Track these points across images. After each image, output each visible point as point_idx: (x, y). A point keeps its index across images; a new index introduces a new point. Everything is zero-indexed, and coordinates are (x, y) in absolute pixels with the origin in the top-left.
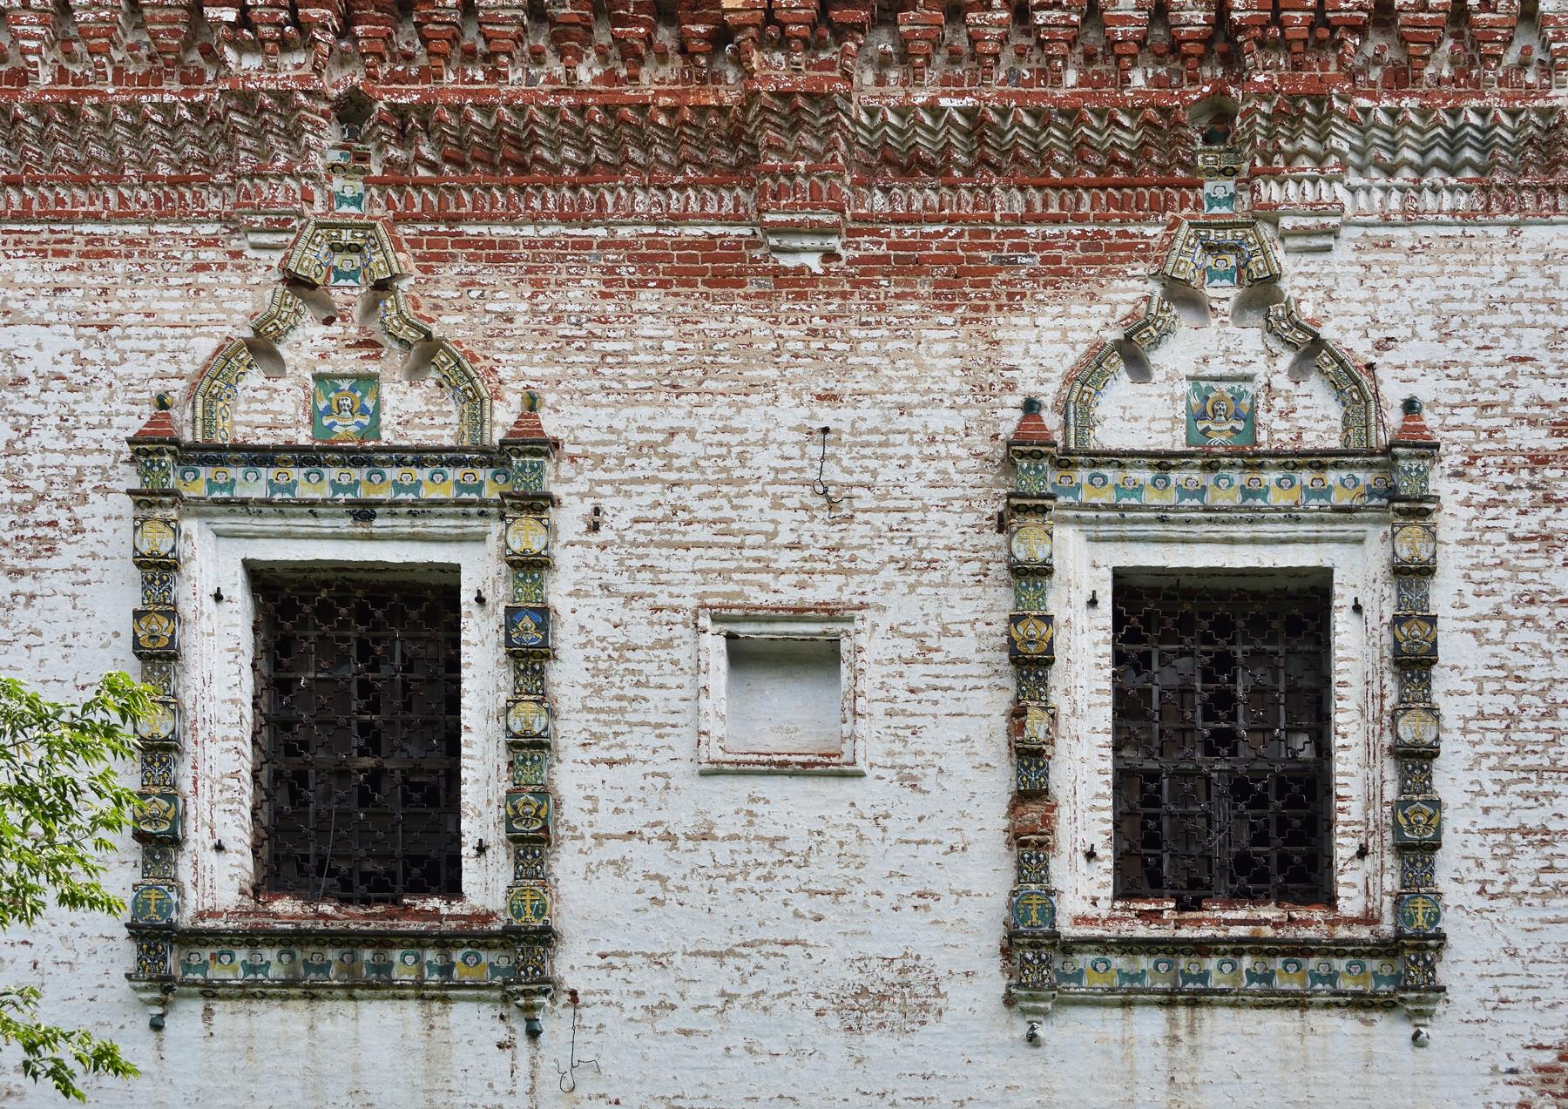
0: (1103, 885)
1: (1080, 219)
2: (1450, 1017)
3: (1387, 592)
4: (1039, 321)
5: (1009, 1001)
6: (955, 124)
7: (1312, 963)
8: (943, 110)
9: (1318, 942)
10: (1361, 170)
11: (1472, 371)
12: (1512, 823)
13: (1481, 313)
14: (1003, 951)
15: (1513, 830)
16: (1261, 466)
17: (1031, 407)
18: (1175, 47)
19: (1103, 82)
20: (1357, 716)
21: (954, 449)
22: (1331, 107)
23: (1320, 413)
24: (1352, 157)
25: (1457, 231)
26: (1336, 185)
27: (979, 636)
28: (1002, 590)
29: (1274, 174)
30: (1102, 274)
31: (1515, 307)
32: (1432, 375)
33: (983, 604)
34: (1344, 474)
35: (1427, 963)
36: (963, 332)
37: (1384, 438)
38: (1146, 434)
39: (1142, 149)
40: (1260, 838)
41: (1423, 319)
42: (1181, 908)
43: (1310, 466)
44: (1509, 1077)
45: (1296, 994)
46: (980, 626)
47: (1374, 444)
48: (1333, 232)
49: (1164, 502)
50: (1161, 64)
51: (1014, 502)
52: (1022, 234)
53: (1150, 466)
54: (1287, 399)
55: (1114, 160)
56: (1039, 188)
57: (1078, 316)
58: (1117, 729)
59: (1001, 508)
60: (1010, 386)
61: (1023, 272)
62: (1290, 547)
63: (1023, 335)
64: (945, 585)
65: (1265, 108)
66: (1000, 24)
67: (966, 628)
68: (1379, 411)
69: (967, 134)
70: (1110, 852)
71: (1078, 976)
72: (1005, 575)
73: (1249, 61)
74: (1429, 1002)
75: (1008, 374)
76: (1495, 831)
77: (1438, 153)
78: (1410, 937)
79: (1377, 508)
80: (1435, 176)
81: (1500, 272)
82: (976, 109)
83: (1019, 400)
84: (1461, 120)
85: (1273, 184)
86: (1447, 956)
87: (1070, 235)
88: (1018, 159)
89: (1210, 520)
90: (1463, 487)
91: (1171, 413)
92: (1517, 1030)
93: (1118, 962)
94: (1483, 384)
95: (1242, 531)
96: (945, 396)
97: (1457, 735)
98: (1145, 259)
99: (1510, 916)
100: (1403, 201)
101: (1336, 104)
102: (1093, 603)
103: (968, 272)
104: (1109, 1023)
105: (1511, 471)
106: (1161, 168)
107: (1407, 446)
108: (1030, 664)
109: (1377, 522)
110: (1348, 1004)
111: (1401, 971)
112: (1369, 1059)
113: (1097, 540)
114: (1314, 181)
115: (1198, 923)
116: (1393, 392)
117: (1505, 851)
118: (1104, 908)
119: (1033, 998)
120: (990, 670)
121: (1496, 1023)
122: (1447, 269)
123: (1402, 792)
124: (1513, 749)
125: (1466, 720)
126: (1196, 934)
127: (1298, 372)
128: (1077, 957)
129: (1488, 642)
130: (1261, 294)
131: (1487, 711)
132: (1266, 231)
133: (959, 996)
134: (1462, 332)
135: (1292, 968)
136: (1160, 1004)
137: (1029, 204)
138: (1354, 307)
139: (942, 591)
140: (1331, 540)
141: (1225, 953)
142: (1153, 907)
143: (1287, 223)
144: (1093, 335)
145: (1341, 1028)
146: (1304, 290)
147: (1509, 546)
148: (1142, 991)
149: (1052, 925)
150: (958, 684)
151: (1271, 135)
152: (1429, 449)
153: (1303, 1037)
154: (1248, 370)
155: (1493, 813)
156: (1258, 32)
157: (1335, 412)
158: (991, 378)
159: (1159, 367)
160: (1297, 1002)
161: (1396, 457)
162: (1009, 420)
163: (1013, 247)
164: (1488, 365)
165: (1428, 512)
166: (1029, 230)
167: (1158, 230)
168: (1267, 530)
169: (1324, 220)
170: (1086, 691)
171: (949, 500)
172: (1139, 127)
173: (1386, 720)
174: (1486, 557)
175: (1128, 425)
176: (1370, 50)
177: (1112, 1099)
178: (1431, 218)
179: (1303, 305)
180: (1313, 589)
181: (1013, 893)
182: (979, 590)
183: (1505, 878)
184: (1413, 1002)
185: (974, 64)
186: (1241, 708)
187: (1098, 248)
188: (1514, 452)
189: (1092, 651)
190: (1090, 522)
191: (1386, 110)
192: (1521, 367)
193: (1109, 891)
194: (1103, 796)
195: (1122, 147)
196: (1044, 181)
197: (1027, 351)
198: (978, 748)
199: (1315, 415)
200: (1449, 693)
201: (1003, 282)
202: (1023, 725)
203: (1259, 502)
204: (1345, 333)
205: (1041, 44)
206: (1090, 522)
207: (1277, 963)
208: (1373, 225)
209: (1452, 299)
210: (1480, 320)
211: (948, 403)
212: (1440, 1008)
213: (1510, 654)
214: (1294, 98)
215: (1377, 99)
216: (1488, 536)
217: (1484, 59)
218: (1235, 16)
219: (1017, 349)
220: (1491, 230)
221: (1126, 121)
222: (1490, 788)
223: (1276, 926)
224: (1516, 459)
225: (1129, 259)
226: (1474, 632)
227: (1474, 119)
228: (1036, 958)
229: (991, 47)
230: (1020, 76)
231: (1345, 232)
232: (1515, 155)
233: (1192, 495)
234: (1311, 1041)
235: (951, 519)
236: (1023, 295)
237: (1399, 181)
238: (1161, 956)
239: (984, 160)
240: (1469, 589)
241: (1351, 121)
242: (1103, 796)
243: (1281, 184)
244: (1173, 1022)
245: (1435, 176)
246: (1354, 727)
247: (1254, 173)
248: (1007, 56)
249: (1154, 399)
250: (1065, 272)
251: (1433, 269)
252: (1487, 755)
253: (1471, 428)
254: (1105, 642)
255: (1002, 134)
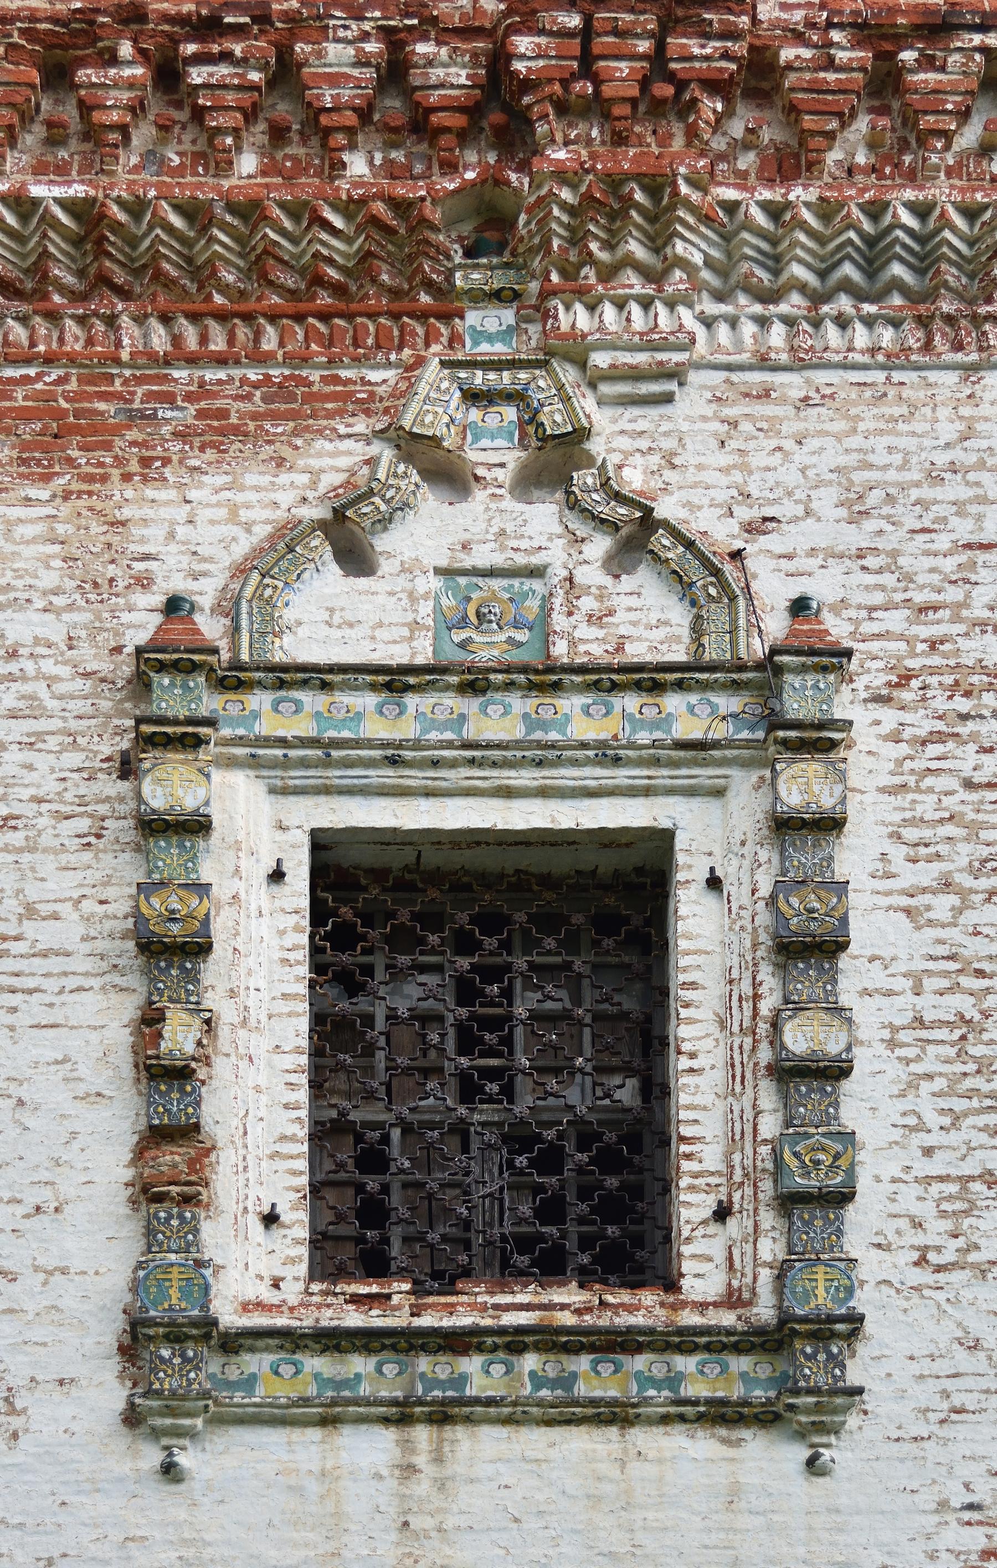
0: (292, 1261)
1: (260, 359)
2: (868, 1433)
3: (763, 855)
4: (193, 494)
5: (132, 1418)
6: (55, 224)
7: (640, 1362)
8: (36, 202)
9: (651, 1331)
10: (720, 297)
11: (901, 561)
12: (970, 1168)
13: (917, 484)
14: (122, 1350)
15: (972, 1178)
16: (556, 687)
17: (174, 606)
18: (420, 124)
19: (300, 168)
20: (714, 1029)
21: (48, 666)
22: (675, 193)
23: (653, 617)
24: (706, 275)
25: (880, 376)
26: (681, 310)
27: (87, 919)
28: (127, 856)
29: (581, 293)
30: (295, 433)
31: (971, 476)
32: (836, 568)
33: (95, 876)
34: (693, 698)
35: (831, 1356)
36: (65, 509)
37: (759, 649)
38: (368, 645)
39: (364, 264)
40: (551, 1210)
41: (822, 492)
42: (419, 1290)
43: (638, 686)
44: (967, 1516)
45: (614, 1403)
46: (89, 906)
47: (743, 653)
48: (676, 374)
49: (397, 736)
50: (395, 145)
51: (147, 729)
52: (166, 379)
53: (373, 687)
54: (600, 598)
55: (318, 280)
56: (194, 317)
57: (257, 489)
58: (316, 1053)
59: (125, 745)
60: (144, 582)
61: (166, 430)
62: (605, 802)
63: (165, 512)
64: (32, 850)
65: (566, 194)
66: (131, 84)
67: (65, 909)
68: (752, 609)
69: (77, 242)
70: (304, 1216)
71: (250, 1382)
72: (131, 836)
73: (541, 129)
74: (835, 1411)
75: (139, 566)
76: (942, 1179)
77: (848, 270)
78: (804, 1320)
79: (747, 744)
80: (844, 303)
81: (948, 430)
82: (90, 202)
83: (158, 600)
84: (887, 219)
85: (579, 307)
86: (862, 1349)
87: (244, 381)
88: (158, 275)
89: (472, 762)
90: (889, 717)
91: (410, 617)
92: (980, 1450)
93: (316, 1363)
94: (920, 579)
95: (525, 778)
96: (35, 596)
97: (881, 1049)
98: (368, 413)
99: (967, 1295)
100: (790, 338)
101: (684, 189)
102: (277, 876)
103: (77, 430)
104: (304, 1448)
105: (967, 694)
106: (395, 293)
107: (798, 653)
108: (171, 952)
109: (745, 764)
110: (700, 1418)
111: (791, 1372)
112: (733, 1495)
113: (285, 791)
114: (646, 304)
115: (451, 1309)
116: (772, 589)
117: (959, 1206)
118: (292, 1292)
119: (171, 1412)
120: (104, 965)
121: (946, 1441)
122: (862, 426)
123: (788, 1124)
124: (971, 1067)
125: (895, 1029)
126: (447, 1322)
127: (619, 563)
128: (246, 1357)
129: (930, 923)
130: (555, 460)
131: (928, 1017)
132: (568, 374)
133: (46, 1415)
134: (886, 510)
135: (606, 1369)
136: (386, 1421)
137: (177, 340)
138: (710, 477)
139: (26, 858)
140: (670, 791)
141: (495, 1348)
142: (375, 1289)
143: (601, 359)
144: (281, 515)
145: (692, 1454)
146: (627, 454)
147: (963, 795)
148: (356, 1402)
149: (205, 1307)
150: (52, 985)
151: (577, 238)
152: (832, 659)
153: (623, 1463)
154: (535, 560)
155: (938, 1155)
156: (557, 87)
157: (679, 616)
158: (111, 570)
159: (389, 555)
160: (615, 1415)
161: (779, 670)
162: (141, 623)
163: (149, 396)
164: (927, 553)
165: (833, 745)
166: (176, 374)
167: (390, 374)
168: (566, 776)
169: (660, 356)
170: (265, 995)
171: (40, 736)
172: (359, 229)
173: (763, 1028)
174: (927, 807)
175: (338, 634)
176: (737, 129)
177: (302, 1553)
178: (837, 358)
179: (626, 472)
180: (639, 871)
181: (140, 1266)
182: (87, 856)
183: (960, 1243)
184: (808, 1411)
185: (88, 146)
186: (519, 1032)
187: (292, 398)
188: (972, 670)
189: (275, 942)
190: (274, 764)
191: (765, 206)
192: (981, 557)
193: (302, 1269)
194: (293, 1139)
195: (330, 261)
196: (203, 307)
197: (171, 535)
198: (83, 1071)
199: (650, 620)
200: (866, 992)
201: (133, 443)
202: (160, 1035)
203: (553, 736)
204: (696, 507)
205: (199, 114)
206: (274, 764)
207: (583, 1363)
208: (741, 368)
209: (871, 466)
210: (915, 494)
211: (40, 604)
212: (853, 1421)
213: (967, 940)
214: (614, 182)
215: (752, 190)
216: (929, 781)
217: (922, 141)
218: (520, 66)
219: (157, 533)
220: (933, 376)
221: (338, 222)
222: (933, 1120)
223: (578, 1312)
224: (975, 679)
225: (340, 413)
226: (908, 911)
227: (907, 218)
228: (172, 1359)
229: (115, 116)
230: (163, 163)
231: (694, 377)
232: (972, 276)
233: (444, 726)
234: (636, 1469)
235: (42, 762)
236: (166, 461)
237: (783, 308)
238: (385, 1355)
239: (104, 280)
240: (898, 853)
241: (708, 219)
242: (293, 1139)
243: (591, 308)
244: (407, 1446)
245: (844, 303)
246: (709, 1043)
247: (547, 293)
248: (143, 135)
249: (381, 599)
250: (236, 431)
251: (840, 426)
252: (929, 1077)
253: (901, 637)
254: (298, 929)
255: (133, 242)
